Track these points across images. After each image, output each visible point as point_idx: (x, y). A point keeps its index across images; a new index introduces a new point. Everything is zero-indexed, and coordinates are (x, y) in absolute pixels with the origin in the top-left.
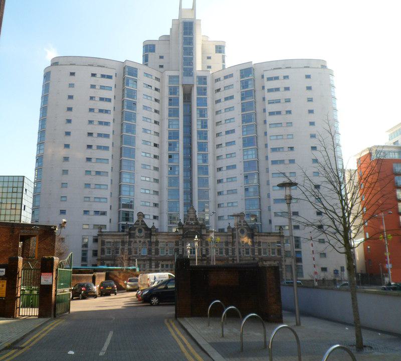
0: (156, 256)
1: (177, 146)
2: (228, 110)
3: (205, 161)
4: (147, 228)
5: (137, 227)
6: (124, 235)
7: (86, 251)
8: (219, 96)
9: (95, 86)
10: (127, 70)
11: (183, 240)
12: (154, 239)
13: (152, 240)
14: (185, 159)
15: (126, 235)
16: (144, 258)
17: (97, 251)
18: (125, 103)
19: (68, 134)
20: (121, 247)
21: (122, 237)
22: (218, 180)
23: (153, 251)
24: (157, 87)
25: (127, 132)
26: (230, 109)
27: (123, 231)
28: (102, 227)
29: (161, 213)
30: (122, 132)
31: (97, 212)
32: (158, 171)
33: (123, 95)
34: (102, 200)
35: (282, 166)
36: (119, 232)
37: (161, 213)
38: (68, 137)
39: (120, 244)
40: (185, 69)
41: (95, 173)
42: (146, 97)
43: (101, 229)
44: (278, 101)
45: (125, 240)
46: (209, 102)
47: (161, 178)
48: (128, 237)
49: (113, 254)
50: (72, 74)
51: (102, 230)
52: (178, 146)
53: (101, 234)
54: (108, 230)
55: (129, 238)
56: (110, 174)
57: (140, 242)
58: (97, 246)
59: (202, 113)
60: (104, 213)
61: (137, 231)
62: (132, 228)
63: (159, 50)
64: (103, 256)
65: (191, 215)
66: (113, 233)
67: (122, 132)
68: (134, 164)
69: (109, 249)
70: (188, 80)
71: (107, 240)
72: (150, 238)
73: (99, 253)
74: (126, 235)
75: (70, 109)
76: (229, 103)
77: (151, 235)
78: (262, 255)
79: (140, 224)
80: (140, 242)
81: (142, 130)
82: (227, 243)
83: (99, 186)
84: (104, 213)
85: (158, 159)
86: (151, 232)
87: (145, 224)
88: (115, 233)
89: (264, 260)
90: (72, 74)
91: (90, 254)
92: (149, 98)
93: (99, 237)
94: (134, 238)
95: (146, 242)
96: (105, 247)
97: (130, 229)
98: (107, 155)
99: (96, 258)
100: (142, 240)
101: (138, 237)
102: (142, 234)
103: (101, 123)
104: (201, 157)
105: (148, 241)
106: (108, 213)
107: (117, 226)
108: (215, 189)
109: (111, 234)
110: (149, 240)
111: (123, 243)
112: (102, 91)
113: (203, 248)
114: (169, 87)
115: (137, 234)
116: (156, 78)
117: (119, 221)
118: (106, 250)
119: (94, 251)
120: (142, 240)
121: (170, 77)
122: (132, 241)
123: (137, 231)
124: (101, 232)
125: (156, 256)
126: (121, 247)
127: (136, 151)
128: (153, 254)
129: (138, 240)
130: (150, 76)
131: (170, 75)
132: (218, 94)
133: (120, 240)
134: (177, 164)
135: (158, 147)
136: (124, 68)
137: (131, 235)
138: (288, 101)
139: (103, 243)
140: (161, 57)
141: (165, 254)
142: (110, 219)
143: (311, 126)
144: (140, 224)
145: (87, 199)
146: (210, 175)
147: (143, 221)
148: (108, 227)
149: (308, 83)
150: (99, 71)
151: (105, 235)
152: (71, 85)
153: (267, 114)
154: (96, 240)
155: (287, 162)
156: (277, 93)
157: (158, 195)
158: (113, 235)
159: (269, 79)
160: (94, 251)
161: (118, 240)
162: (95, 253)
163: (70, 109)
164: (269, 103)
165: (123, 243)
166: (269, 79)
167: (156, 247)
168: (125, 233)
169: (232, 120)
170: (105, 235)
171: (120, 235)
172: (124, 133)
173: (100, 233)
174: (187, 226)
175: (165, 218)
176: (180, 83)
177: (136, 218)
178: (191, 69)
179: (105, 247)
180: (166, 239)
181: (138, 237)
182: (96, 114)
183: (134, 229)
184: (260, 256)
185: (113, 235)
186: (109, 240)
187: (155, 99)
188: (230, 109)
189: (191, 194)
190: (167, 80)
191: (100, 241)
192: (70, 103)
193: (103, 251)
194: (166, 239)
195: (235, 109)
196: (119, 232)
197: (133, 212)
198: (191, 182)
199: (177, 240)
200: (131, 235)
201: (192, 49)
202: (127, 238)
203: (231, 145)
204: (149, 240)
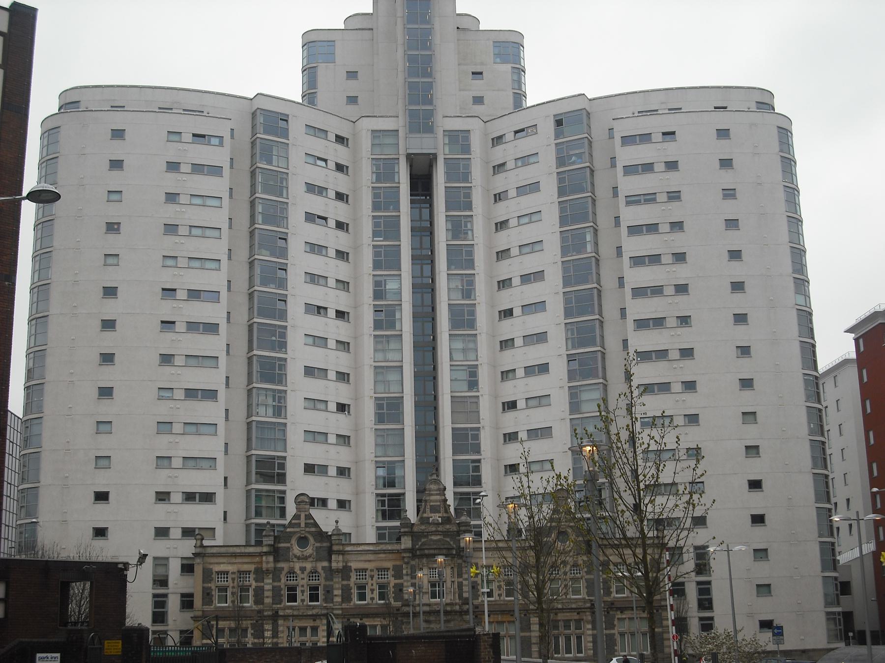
0: (344, 606)
1: (396, 170)
2: (525, 220)
3: (468, 292)
4: (321, 535)
5: (295, 533)
6: (261, 555)
7: (165, 596)
8: (504, 240)
9: (168, 493)
10: (260, 119)
11: (413, 563)
12: (337, 562)
13: (334, 565)
14: (416, 346)
15: (266, 554)
16: (314, 612)
17: (191, 595)
18: (259, 208)
19: (110, 292)
20: (254, 584)
21: (257, 559)
22: (503, 404)
23: (336, 592)
24: (342, 190)
25: (263, 284)
26: (532, 216)
27: (259, 543)
28: (202, 533)
29: (357, 493)
30: (251, 286)
31: (189, 497)
32: (348, 351)
33: (253, 186)
34: (210, 202)
35: (662, 365)
36: (247, 545)
37: (357, 493)
38: (107, 369)
39: (252, 576)
40: (412, 114)
41: (180, 531)
42: (311, 160)
43: (202, 539)
44: (650, 198)
45: (264, 566)
46: (478, 199)
47: (356, 338)
48: (271, 558)
49: (233, 602)
50: (118, 134)
51: (206, 543)
52: (398, 316)
53: (201, 553)
54: (219, 540)
55: (276, 561)
56: (226, 171)
57: (303, 569)
58: (192, 584)
59: (459, 228)
60: (208, 498)
61: (294, 541)
62: (282, 536)
63: (345, 57)
64: (206, 608)
65: (433, 498)
66: (231, 550)
67: (253, 192)
68: (284, 431)
69: (223, 589)
70: (422, 145)
71: (217, 568)
72: (330, 561)
73: (198, 602)
74: (266, 554)
75: (107, 358)
76: (528, 203)
77: (330, 552)
78: (614, 595)
79: (303, 525)
80: (303, 569)
81: (304, 188)
82: (525, 569)
83: (195, 427)
84: (208, 498)
85: (347, 174)
86: (332, 545)
87: (316, 525)
88: (238, 550)
89: (618, 609)
90: (118, 134)
91: (173, 604)
92: (320, 163)
93: (198, 560)
94: (287, 560)
95: (320, 570)
96: (212, 585)
97: (277, 539)
98: (217, 186)
99: (188, 615)
100: (309, 566)
101: (299, 558)
102: (309, 550)
103: (192, 326)
104: (457, 283)
105: (323, 568)
106: (219, 498)
107: (243, 529)
108: (497, 427)
109: (229, 553)
110: (325, 564)
111: (260, 574)
112: (196, 177)
113: (465, 583)
114: (378, 528)
115: (296, 550)
116: (337, 136)
117: (248, 483)
118: (216, 594)
119: (183, 595)
120: (309, 566)
121: (376, 133)
122: (283, 568)
123: (294, 541)
124: (202, 546)
125: (344, 606)
126: (254, 584)
127: (291, 209)
128: (338, 599)
129: (297, 566)
130: (322, 281)
131: (375, 128)
132: (503, 234)
133: (252, 567)
134: (400, 459)
135: (348, 321)
136: (254, 115)
137: (276, 553)
138: (674, 196)
139: (207, 575)
140: (352, 75)
141: (368, 601)
142: (225, 513)
143: (730, 233)
144: (303, 525)
145: (170, 262)
146: (478, 299)
147: (309, 516)
148: (219, 533)
149: (724, 149)
150: (190, 125)
151: (214, 555)
152: (111, 258)
153: (624, 230)
154: (187, 568)
155: (674, 355)
156: (649, 176)
157: (348, 291)
158: (234, 555)
159: (628, 140)
160: (183, 595)
161: (246, 567)
162: (187, 602)
163: (109, 325)
164: (628, 203)
165: (260, 574)
166: (628, 140)
167: (345, 583)
168: (265, 549)
169: (534, 218)
170: (214, 555)
171: (249, 555)
172: (256, 288)
173: (199, 550)
174: (423, 527)
175: (369, 507)
176: (402, 151)
177: (291, 509)
178: (430, 114)
179: (212, 585)
180: (369, 561)
181: (299, 558)
182: (182, 305)
183: (288, 537)
184: (606, 599)
185: (234, 555)
186: (223, 568)
187: (338, 251)
188: (532, 216)
189: (432, 260)
190: (366, 142)
191: (198, 570)
192: (108, 342)
193: (207, 595)
194: (369, 561)
195: (542, 186)
196: (247, 545)
197: (284, 492)
198: (432, 348)
199: (398, 563)
200: (276, 553)
201: (429, 60)
202: (268, 562)
203: (536, 312)
204: (325, 564)
